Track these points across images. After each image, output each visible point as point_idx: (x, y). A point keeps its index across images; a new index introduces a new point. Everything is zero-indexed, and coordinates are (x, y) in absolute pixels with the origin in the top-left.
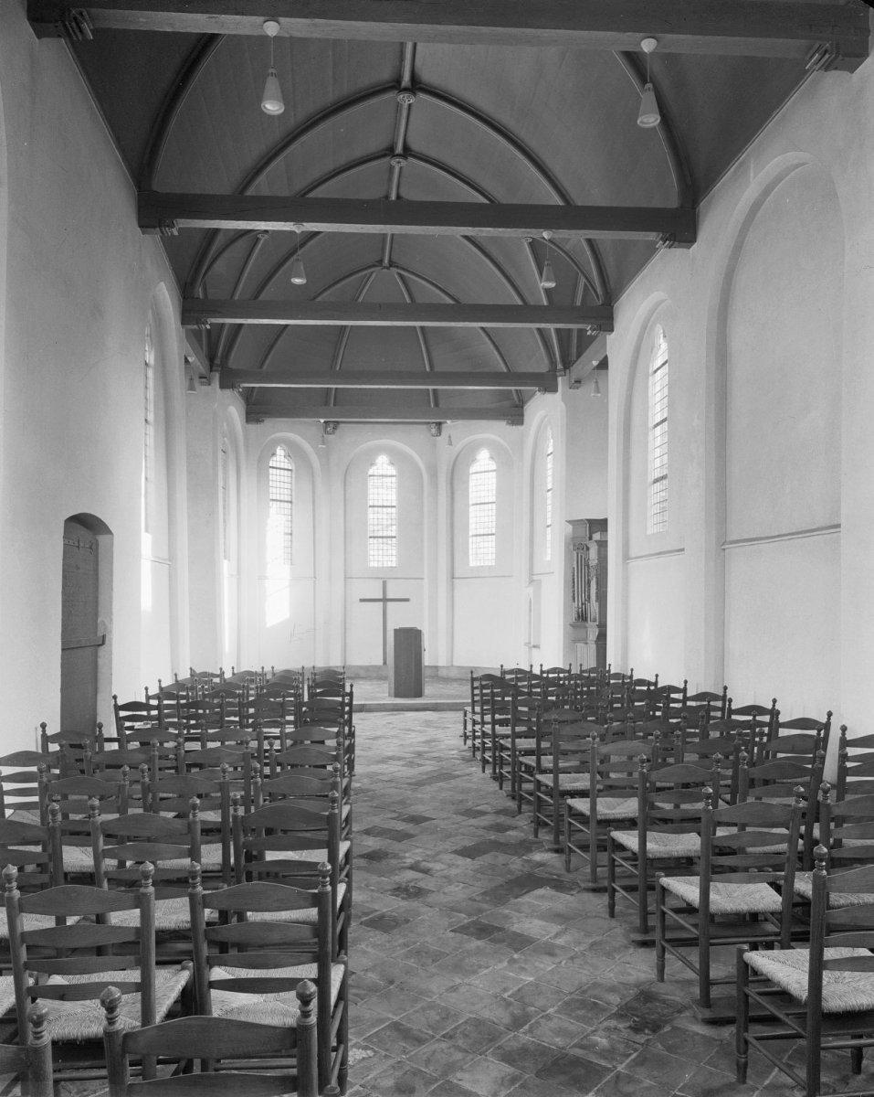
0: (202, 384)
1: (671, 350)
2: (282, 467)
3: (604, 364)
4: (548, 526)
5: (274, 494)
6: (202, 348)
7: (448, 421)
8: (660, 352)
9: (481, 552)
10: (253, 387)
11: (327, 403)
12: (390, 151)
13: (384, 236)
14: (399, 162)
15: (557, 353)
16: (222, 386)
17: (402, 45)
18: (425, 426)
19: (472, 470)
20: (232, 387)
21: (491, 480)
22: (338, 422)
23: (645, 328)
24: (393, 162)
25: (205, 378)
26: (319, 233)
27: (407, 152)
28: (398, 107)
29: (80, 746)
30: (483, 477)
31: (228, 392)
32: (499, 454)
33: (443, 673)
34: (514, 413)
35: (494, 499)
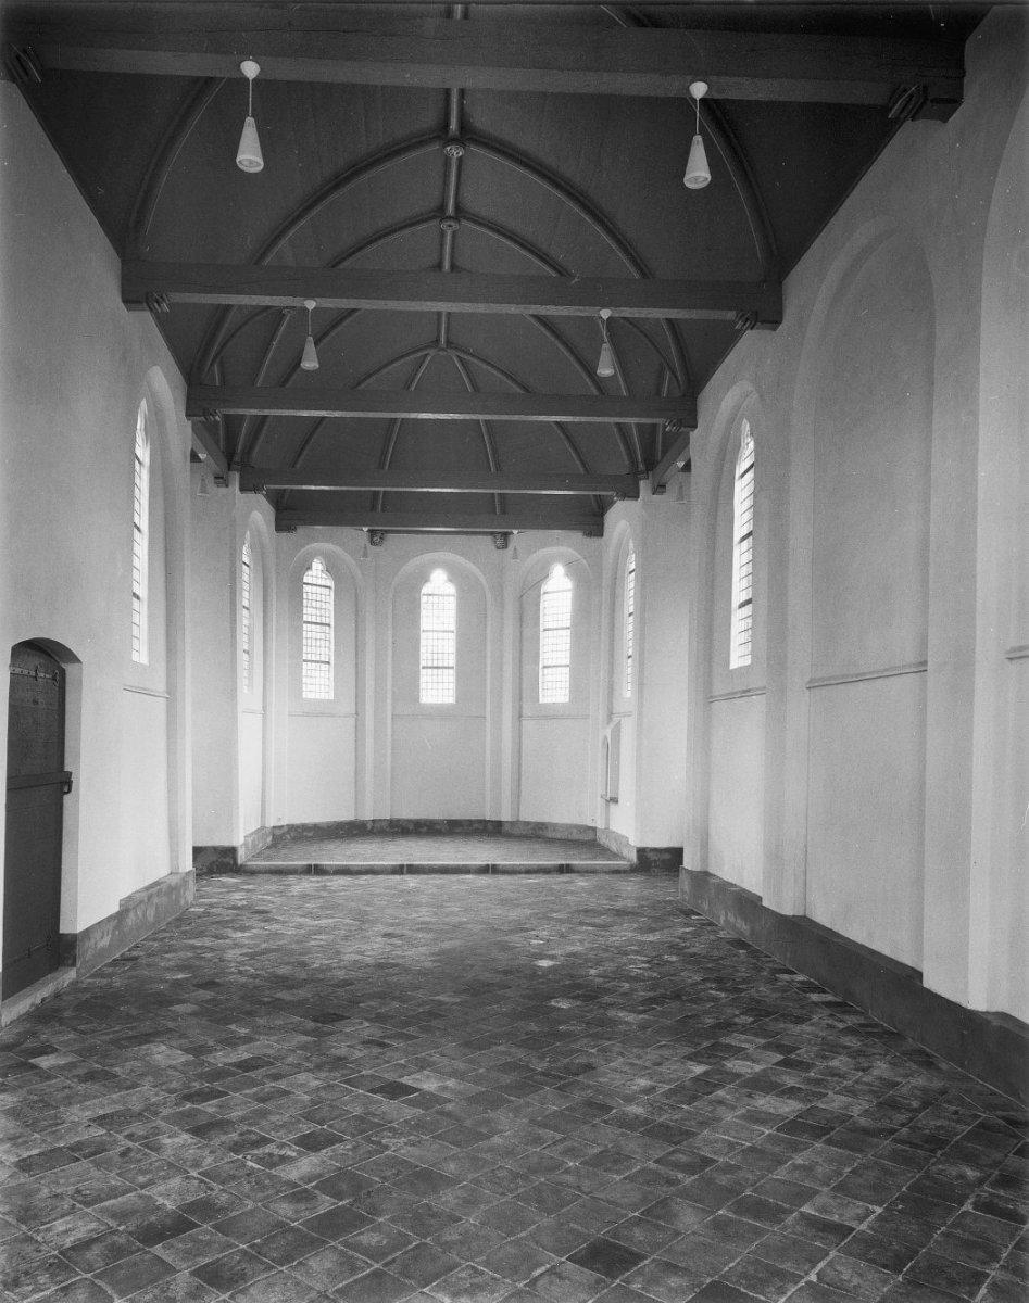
0: (218, 485)
1: (758, 451)
2: (315, 588)
3: (687, 467)
4: (629, 657)
5: (309, 613)
6: (217, 442)
7: (516, 532)
8: (748, 452)
9: (555, 687)
10: (284, 490)
11: (373, 508)
12: (439, 212)
13: (439, 314)
14: (450, 226)
15: (639, 452)
16: (243, 489)
17: (447, 92)
18: (490, 537)
19: (425, 590)
20: (256, 489)
21: (329, 597)
22: (386, 532)
23: (733, 422)
24: (444, 226)
25: (222, 478)
26: (354, 311)
27: (461, 213)
28: (447, 161)
29: (987, 1207)
30: (558, 595)
31: (251, 496)
32: (573, 569)
33: (506, 828)
34: (591, 520)
35: (569, 625)
